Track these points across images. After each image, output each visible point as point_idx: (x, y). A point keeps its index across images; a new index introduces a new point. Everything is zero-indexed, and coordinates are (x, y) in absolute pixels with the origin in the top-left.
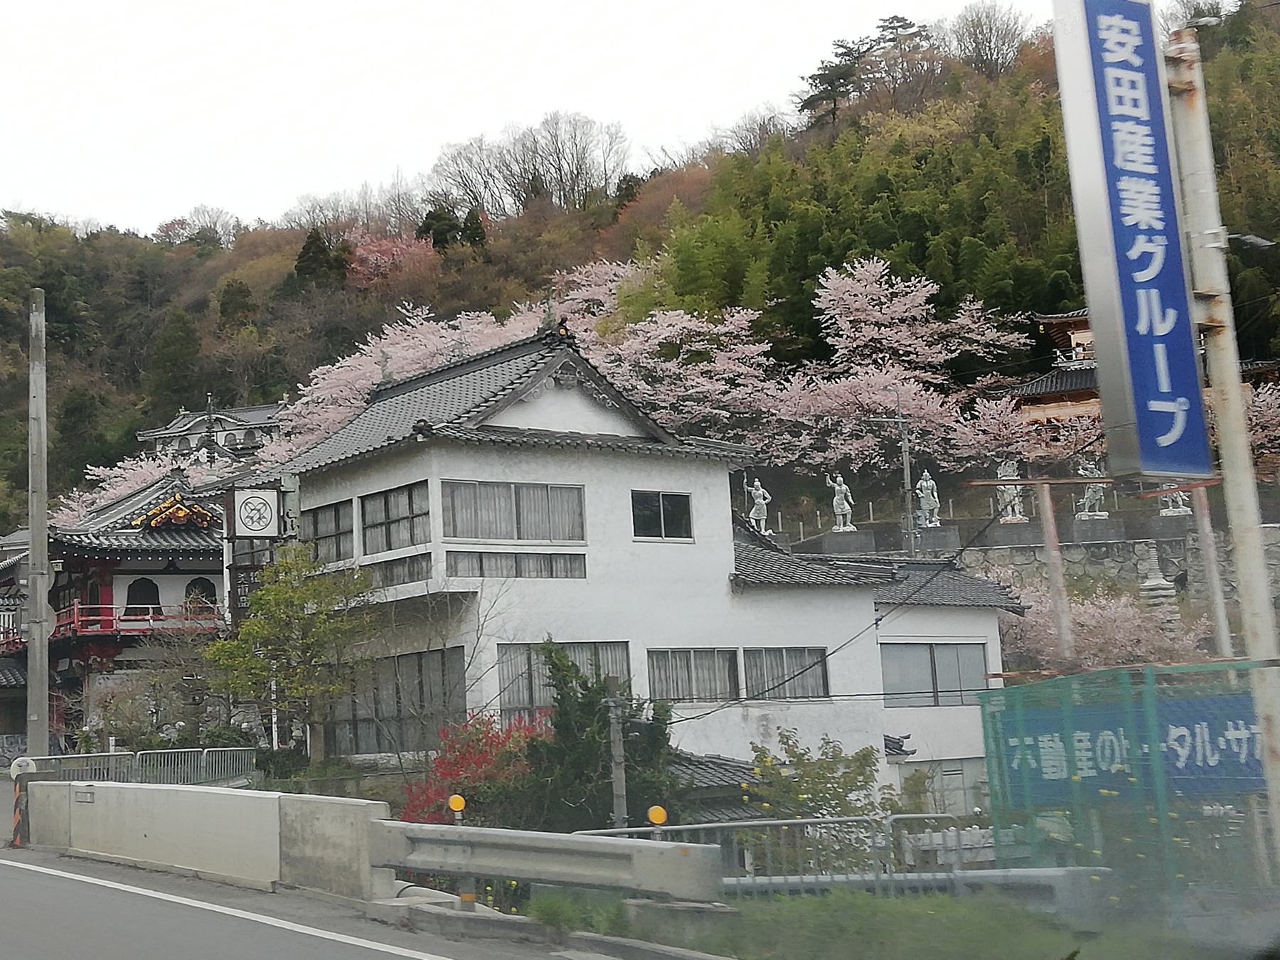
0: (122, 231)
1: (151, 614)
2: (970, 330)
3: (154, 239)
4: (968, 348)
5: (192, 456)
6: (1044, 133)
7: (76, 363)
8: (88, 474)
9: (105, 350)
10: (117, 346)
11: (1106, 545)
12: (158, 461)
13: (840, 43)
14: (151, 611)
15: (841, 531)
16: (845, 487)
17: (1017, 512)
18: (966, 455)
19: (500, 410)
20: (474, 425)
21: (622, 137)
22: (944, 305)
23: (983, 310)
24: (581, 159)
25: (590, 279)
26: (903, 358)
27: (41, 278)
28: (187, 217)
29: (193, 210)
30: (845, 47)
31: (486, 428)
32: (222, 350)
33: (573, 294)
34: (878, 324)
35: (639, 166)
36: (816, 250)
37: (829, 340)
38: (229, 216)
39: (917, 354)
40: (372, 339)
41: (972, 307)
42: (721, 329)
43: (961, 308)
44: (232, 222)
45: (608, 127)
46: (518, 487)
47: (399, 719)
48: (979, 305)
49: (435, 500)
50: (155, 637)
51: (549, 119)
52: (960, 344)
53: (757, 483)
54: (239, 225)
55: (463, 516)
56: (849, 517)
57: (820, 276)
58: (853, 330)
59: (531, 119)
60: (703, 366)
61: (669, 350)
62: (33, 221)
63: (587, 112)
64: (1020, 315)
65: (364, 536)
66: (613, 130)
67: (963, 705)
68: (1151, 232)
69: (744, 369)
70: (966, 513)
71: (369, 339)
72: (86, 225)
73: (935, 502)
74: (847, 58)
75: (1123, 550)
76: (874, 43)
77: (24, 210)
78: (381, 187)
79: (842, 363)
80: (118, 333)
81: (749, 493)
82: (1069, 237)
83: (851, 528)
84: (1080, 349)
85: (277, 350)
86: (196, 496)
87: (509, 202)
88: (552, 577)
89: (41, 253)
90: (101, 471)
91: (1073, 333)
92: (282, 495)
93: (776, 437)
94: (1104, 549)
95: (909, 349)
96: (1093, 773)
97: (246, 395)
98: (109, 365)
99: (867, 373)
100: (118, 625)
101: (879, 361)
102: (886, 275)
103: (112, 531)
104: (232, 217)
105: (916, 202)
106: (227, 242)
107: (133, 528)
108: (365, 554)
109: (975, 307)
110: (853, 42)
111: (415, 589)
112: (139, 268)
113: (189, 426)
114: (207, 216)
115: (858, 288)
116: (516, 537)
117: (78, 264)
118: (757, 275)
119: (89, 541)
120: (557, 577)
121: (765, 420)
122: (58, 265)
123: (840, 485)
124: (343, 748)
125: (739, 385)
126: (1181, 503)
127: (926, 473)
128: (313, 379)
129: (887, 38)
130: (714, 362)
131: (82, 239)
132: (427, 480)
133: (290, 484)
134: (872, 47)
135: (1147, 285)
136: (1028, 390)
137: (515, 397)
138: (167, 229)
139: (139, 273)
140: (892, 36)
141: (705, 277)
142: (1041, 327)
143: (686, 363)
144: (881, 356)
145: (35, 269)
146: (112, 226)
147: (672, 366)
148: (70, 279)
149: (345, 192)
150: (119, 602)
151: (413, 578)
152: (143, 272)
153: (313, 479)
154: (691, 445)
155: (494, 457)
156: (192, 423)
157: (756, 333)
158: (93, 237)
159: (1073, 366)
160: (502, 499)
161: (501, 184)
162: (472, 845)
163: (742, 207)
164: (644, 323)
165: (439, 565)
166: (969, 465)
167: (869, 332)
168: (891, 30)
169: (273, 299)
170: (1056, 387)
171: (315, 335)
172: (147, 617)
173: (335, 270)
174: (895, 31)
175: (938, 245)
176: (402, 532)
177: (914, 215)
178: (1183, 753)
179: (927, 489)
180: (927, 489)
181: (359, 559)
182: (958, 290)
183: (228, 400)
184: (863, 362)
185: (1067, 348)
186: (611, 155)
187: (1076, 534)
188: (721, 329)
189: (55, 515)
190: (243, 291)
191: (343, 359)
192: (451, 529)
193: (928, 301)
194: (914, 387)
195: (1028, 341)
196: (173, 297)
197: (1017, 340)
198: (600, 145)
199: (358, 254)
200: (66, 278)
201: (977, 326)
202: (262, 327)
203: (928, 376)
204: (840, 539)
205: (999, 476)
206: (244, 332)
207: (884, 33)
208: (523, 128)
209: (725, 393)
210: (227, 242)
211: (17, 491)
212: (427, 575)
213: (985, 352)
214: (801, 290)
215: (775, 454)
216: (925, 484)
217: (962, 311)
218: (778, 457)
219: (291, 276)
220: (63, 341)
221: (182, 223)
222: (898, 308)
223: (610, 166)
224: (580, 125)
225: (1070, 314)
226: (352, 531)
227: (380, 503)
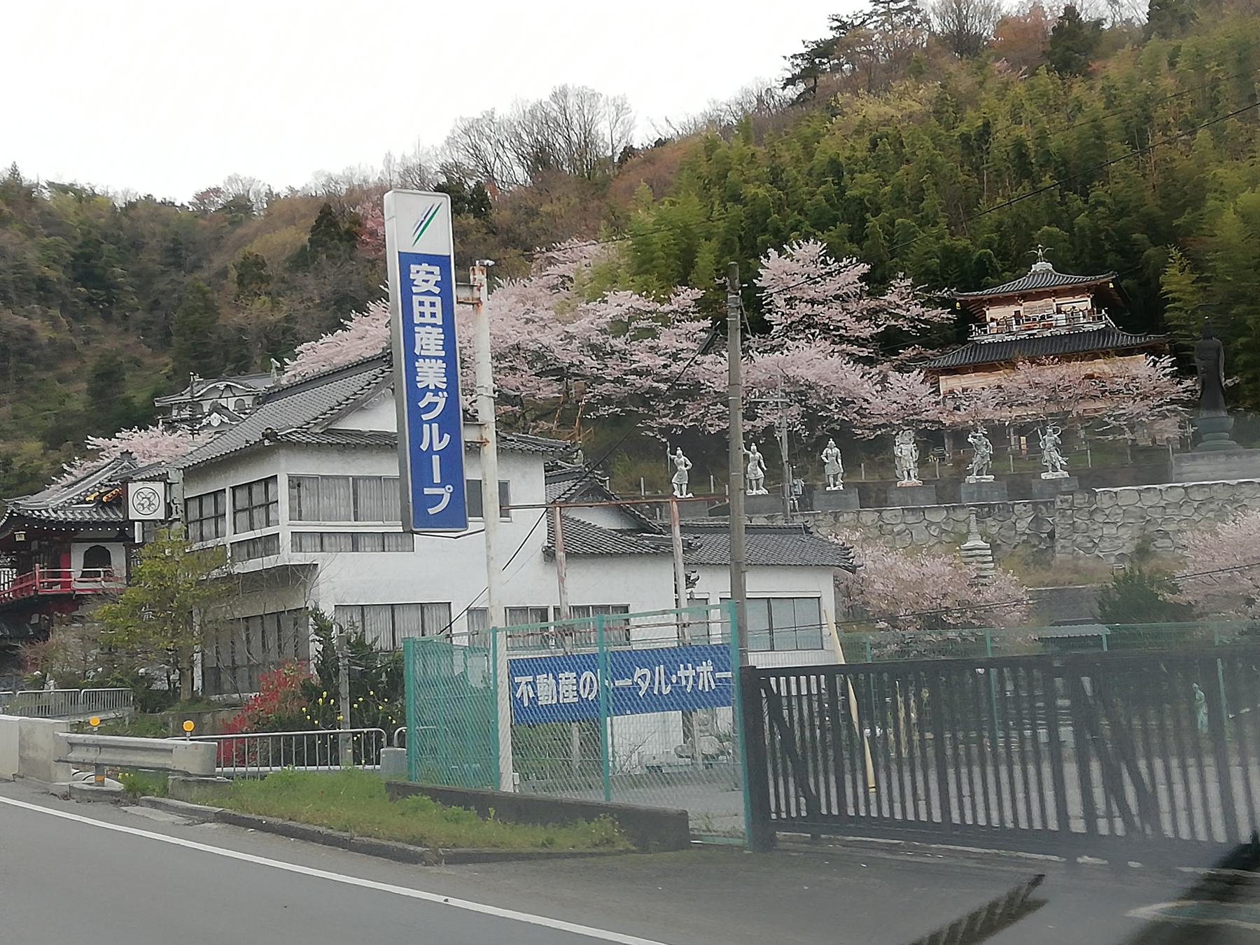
0: (159, 200)
1: (102, 577)
2: (898, 306)
3: (190, 207)
4: (893, 323)
5: (204, 420)
6: (985, 117)
7: (114, 328)
8: (89, 444)
9: (140, 315)
10: (151, 310)
11: (989, 506)
12: (151, 433)
13: (835, 18)
14: (102, 573)
15: (754, 494)
16: (758, 454)
17: (912, 475)
18: (880, 423)
19: (346, 415)
20: (321, 429)
21: (628, 109)
22: (876, 282)
23: (913, 286)
24: (587, 132)
25: (567, 255)
26: (834, 333)
27: (80, 247)
28: (221, 185)
29: (227, 178)
30: (840, 21)
31: (331, 431)
32: (238, 319)
33: (551, 269)
34: (813, 302)
35: (642, 138)
36: (764, 231)
37: (767, 317)
38: (261, 184)
39: (846, 329)
40: (356, 315)
41: (902, 284)
42: (666, 308)
43: (892, 285)
44: (264, 190)
45: (614, 99)
46: (355, 479)
47: (234, 669)
48: (909, 282)
49: (282, 491)
50: (102, 596)
51: (558, 92)
52: (886, 319)
53: (679, 452)
54: (271, 192)
55: (307, 505)
56: (761, 481)
57: (762, 257)
58: (788, 307)
59: (538, 92)
60: (648, 342)
61: (619, 327)
62: (75, 192)
63: (593, 84)
64: (946, 292)
65: (235, 518)
66: (619, 102)
67: (797, 649)
68: (436, 391)
69: (685, 345)
70: (877, 477)
71: (353, 316)
72: (126, 193)
73: (839, 468)
74: (842, 31)
75: (1003, 509)
76: (866, 17)
77: (66, 181)
78: (404, 156)
79: (779, 337)
80: (152, 299)
81: (672, 460)
82: (998, 217)
83: (764, 491)
84: (994, 324)
85: (288, 319)
86: (112, 483)
87: (520, 174)
88: (384, 551)
89: (81, 223)
90: (100, 441)
91: (988, 309)
92: (169, 486)
93: (711, 407)
94: (986, 509)
95: (839, 324)
96: (576, 700)
97: (259, 362)
98: (145, 329)
99: (797, 347)
100: (76, 586)
101: (809, 336)
102: (822, 255)
103: (69, 506)
104: (264, 185)
105: (861, 184)
106: (259, 207)
107: (87, 503)
108: (235, 533)
109: (905, 284)
110: (847, 16)
111: (269, 562)
112: (173, 236)
113: (202, 392)
114: (240, 184)
115: (795, 267)
116: (352, 518)
117: (116, 232)
118: (706, 256)
119: (46, 515)
120: (389, 551)
121: (703, 391)
122: (96, 234)
123: (754, 453)
124: (226, 688)
125: (681, 359)
126: (1059, 467)
127: (831, 441)
128: (298, 355)
129: (879, 12)
130: (658, 338)
131: (121, 208)
132: (276, 476)
133: (175, 477)
134: (864, 21)
135: (430, 422)
136: (944, 362)
137: (356, 405)
138: (202, 197)
139: (174, 240)
140: (883, 10)
141: (658, 257)
142: (958, 304)
143: (634, 338)
144: (813, 331)
145: (75, 238)
146: (149, 195)
147: (619, 343)
148: (107, 247)
149: (359, 166)
150: (77, 565)
151: (267, 554)
152: (177, 240)
153: (194, 472)
154: (513, 440)
155: (336, 455)
156: (205, 390)
157: (705, 309)
158: (131, 206)
159: (988, 339)
160: (342, 489)
161: (512, 155)
162: (100, 747)
163: (705, 188)
164: (595, 303)
165: (285, 540)
166: (879, 433)
167: (804, 309)
168: (882, 5)
169: (286, 270)
170: (969, 359)
171: (324, 305)
172: (99, 579)
173: (345, 243)
174: (887, 5)
175: (874, 226)
176: (259, 515)
177: (854, 198)
178: (644, 686)
179: (832, 456)
180: (832, 456)
181: (230, 538)
182: (891, 269)
183: (242, 367)
184: (797, 337)
185: (982, 323)
186: (617, 125)
187: (963, 496)
188: (666, 308)
189: (59, 481)
190: (259, 263)
191: (327, 335)
192: (297, 513)
193: (861, 279)
194: (836, 360)
195: (950, 316)
196: (205, 264)
197: (939, 314)
198: (607, 116)
199: (368, 226)
200: (103, 246)
201: (904, 302)
202: (274, 297)
203: (854, 349)
204: (758, 501)
205: (897, 444)
206: (258, 304)
207: (876, 7)
208: (533, 101)
209: (665, 366)
210: (259, 207)
211: (50, 451)
212: (276, 550)
213: (909, 327)
214: (749, 269)
215: (708, 422)
216: (830, 451)
217: (893, 288)
218: (711, 425)
219: (304, 248)
220: (101, 307)
221: (217, 191)
222: (830, 287)
223: (617, 136)
224: (588, 98)
225: (985, 291)
226: (225, 515)
227: (245, 492)
